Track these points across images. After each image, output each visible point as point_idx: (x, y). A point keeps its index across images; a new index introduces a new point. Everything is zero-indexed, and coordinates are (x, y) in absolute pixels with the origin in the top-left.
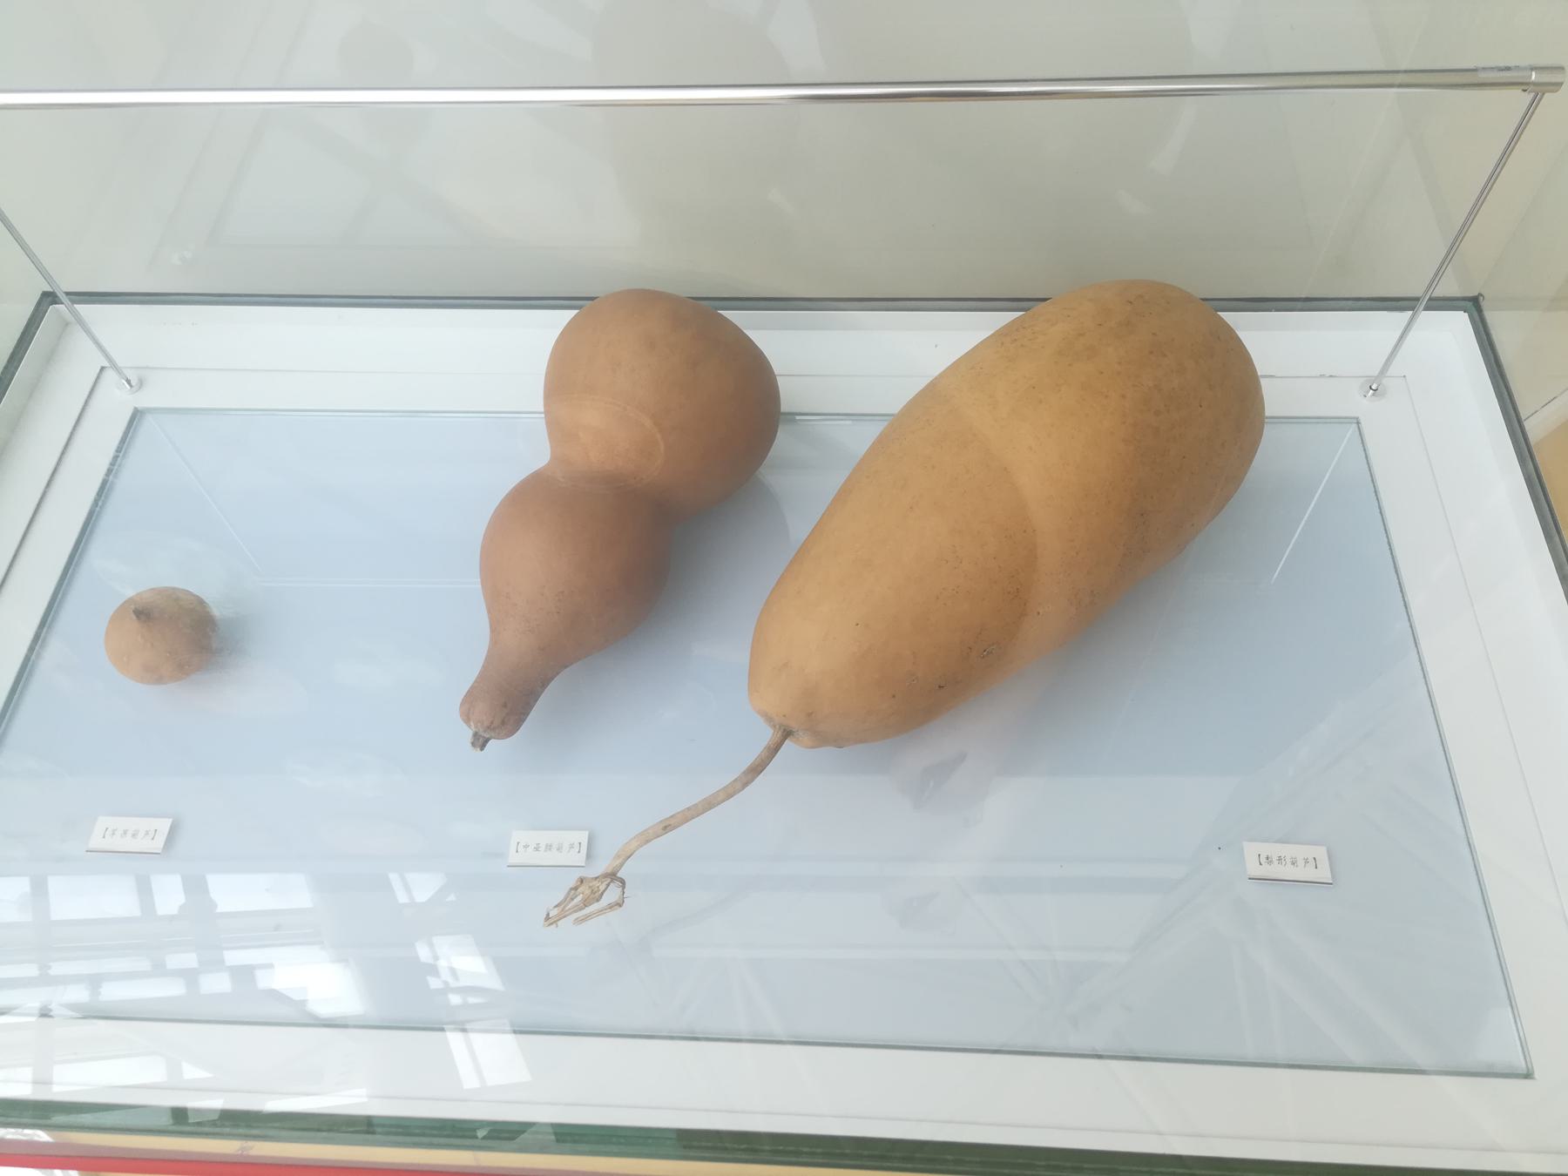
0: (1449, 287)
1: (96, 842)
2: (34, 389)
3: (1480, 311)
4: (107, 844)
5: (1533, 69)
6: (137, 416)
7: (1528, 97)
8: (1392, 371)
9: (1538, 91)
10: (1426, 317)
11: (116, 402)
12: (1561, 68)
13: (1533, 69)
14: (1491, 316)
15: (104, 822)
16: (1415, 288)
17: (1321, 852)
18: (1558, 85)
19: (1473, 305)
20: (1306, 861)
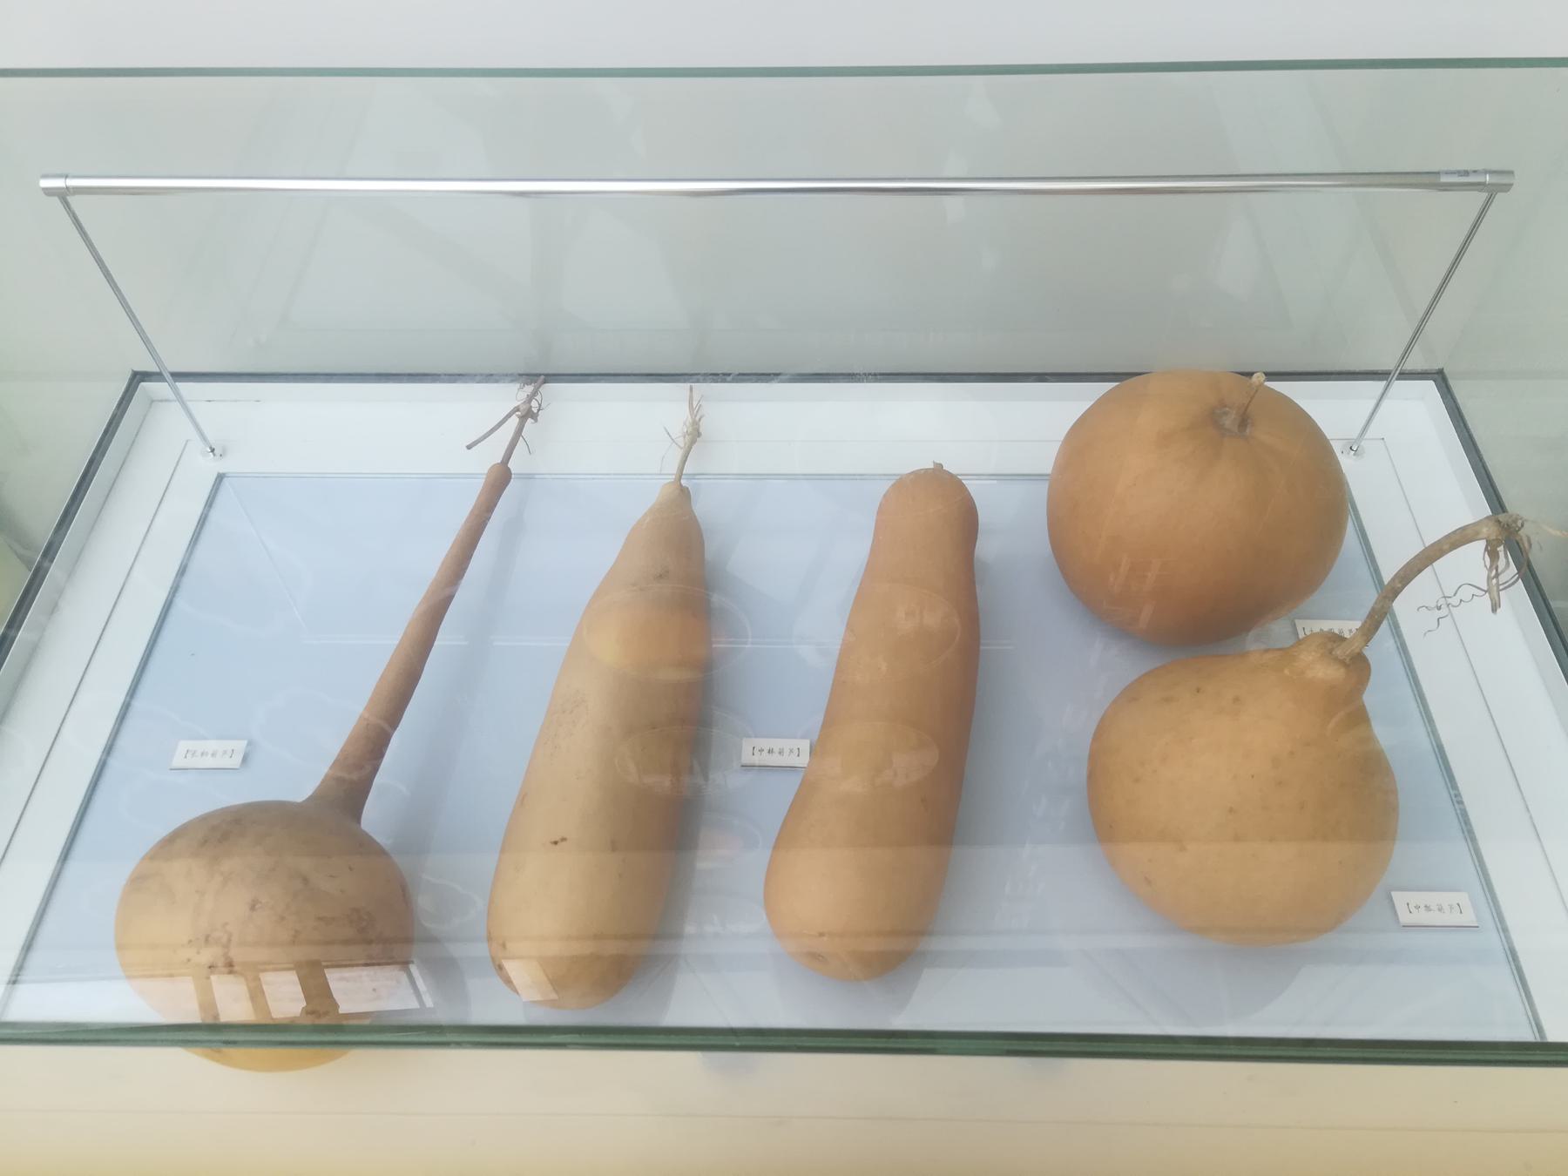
0: (1415, 362)
1: (178, 761)
2: (34, 650)
3: (1445, 379)
4: (191, 762)
5: (1486, 172)
6: (220, 478)
7: (1484, 195)
8: (1368, 435)
9: (1492, 191)
10: (1399, 386)
11: (205, 469)
12: (1511, 173)
13: (1486, 172)
14: (1459, 389)
15: (184, 745)
16: (1388, 364)
17: (1405, 918)
18: (1506, 187)
19: (1440, 378)
20: (1451, 907)
